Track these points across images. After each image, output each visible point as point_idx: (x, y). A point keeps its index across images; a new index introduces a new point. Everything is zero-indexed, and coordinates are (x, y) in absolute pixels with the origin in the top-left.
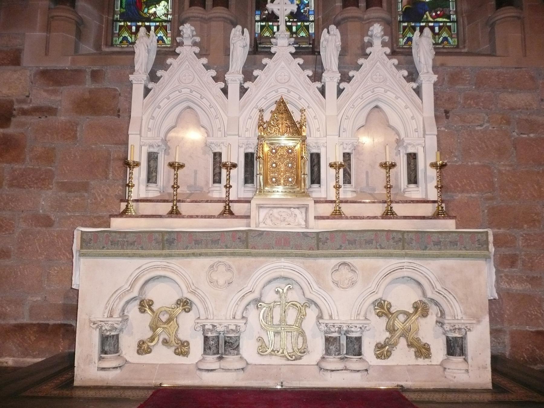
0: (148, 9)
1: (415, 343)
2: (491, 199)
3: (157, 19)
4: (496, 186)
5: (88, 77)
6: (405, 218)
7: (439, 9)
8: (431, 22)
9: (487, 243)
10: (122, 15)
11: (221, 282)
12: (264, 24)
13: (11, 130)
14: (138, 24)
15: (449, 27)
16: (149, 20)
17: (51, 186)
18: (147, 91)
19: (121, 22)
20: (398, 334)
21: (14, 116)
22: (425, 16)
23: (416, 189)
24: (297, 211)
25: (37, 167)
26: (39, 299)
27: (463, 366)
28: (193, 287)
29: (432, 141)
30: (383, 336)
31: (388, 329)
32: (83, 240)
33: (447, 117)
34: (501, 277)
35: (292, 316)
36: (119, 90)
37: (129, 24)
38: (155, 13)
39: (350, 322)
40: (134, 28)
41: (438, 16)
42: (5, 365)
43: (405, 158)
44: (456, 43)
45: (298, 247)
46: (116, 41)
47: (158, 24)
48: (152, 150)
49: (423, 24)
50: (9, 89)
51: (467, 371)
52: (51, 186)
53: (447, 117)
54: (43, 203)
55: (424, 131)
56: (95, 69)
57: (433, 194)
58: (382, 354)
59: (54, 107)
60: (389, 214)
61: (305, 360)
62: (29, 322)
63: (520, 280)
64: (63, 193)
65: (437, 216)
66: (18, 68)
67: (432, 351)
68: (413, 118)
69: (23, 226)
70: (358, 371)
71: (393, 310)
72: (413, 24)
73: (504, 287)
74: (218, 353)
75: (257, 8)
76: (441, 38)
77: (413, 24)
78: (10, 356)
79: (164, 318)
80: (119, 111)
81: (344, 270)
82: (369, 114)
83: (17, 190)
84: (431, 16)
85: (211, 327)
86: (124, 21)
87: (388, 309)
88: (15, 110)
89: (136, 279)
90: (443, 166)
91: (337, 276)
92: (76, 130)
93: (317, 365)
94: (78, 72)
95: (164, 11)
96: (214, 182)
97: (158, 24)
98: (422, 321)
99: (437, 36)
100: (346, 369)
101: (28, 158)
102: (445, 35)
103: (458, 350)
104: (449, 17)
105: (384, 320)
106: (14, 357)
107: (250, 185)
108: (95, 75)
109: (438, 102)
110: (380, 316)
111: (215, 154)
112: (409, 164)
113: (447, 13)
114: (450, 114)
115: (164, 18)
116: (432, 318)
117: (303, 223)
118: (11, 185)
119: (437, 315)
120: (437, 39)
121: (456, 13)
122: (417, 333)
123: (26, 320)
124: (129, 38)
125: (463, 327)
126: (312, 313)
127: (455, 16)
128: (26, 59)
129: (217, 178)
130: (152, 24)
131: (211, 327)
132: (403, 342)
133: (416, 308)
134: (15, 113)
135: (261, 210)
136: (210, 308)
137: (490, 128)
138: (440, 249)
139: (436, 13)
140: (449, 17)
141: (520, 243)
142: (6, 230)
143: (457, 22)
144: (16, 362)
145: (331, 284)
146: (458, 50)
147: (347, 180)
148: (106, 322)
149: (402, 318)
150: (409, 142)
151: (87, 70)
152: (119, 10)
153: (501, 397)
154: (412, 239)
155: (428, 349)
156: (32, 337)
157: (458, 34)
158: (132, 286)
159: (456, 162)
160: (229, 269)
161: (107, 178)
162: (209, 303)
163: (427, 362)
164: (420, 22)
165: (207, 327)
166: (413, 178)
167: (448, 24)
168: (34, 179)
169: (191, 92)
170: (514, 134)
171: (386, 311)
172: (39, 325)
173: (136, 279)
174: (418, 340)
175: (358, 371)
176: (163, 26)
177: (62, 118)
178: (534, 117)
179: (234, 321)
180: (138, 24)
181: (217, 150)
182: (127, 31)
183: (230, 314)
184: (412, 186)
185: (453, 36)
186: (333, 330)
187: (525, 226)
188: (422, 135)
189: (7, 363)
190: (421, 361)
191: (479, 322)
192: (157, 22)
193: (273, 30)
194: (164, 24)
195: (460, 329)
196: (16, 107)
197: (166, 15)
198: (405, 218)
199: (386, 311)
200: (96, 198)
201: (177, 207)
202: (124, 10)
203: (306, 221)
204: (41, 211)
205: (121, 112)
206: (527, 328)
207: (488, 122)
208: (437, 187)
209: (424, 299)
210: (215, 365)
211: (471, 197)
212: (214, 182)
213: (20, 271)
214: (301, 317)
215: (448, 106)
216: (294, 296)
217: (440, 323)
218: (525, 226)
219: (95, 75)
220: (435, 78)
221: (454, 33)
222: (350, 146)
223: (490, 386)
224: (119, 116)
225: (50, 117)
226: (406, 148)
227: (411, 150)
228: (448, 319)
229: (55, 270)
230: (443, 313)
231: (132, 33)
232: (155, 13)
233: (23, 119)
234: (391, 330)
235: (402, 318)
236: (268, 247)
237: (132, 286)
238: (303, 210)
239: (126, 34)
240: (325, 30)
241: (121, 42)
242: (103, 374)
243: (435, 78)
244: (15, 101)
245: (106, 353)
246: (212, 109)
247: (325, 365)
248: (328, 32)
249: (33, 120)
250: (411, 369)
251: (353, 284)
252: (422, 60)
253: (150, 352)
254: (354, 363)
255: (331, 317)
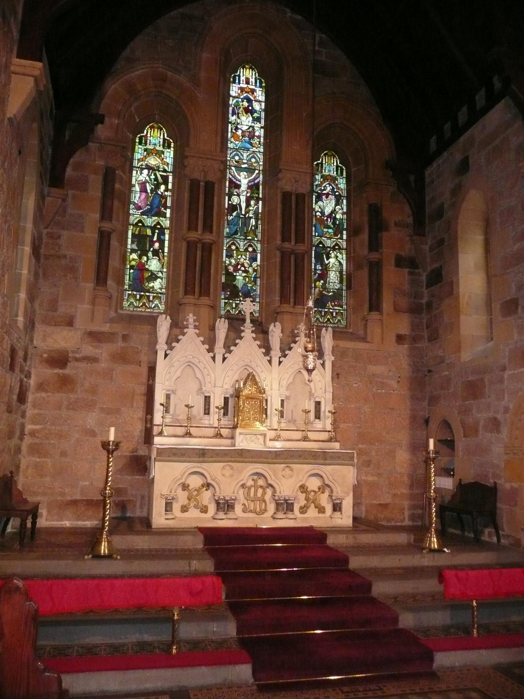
0: (148, 284)
1: (319, 507)
2: (360, 427)
3: (154, 292)
4: (363, 420)
5: (120, 339)
6: (315, 441)
7: (336, 300)
8: (332, 309)
9: (353, 457)
10: (130, 285)
11: (227, 475)
12: (227, 301)
13: (67, 371)
14: (141, 294)
15: (342, 313)
16: (149, 292)
17: (95, 410)
18: (166, 355)
19: (129, 291)
20: (311, 501)
21: (70, 362)
22: (328, 305)
23: (319, 422)
24: (260, 437)
25: (86, 397)
26: (88, 483)
27: (340, 516)
28: (214, 477)
29: (329, 396)
30: (303, 503)
31: (306, 499)
32: (157, 453)
33: (338, 378)
34: (362, 473)
35: (260, 491)
36: (140, 348)
37: (135, 293)
38: (153, 287)
39: (289, 495)
40: (138, 297)
41: (335, 305)
42: (64, 526)
43: (314, 403)
44: (345, 324)
45: (266, 458)
46: (125, 304)
47: (155, 295)
48: (168, 393)
49: (327, 310)
50: (66, 343)
51: (342, 518)
52: (95, 410)
53: (338, 378)
54: (90, 421)
55: (325, 390)
56: (125, 333)
57: (329, 427)
58: (303, 511)
59: (97, 357)
60: (305, 439)
61: (266, 515)
62: (80, 498)
63: (373, 475)
64: (103, 415)
65: (330, 440)
66: (71, 328)
67: (326, 510)
68: (320, 381)
69: (77, 436)
70: (292, 519)
71: (309, 490)
72: (320, 310)
73: (364, 478)
74: (224, 511)
75: (223, 291)
76: (337, 320)
77: (320, 310)
78: (68, 520)
79: (195, 493)
80: (140, 362)
81: (287, 470)
82: (295, 375)
83: (72, 412)
84: (332, 305)
85: (223, 498)
86: (132, 291)
87: (307, 489)
88: (70, 357)
89: (184, 473)
90: (334, 413)
91: (284, 473)
92: (113, 374)
93: (272, 517)
94: (113, 334)
95: (159, 286)
96: (205, 414)
97: (155, 295)
98: (322, 495)
99: (334, 319)
100: (287, 518)
101: (79, 391)
102: (339, 318)
103: (338, 509)
104: (342, 307)
105: (304, 495)
106: (70, 521)
107: (227, 417)
108: (125, 338)
109: (334, 368)
110: (302, 493)
111: (206, 397)
112: (316, 407)
113: (341, 303)
114: (340, 376)
115: (159, 291)
116: (327, 494)
117: (263, 443)
118: (68, 408)
119: (329, 492)
120: (334, 321)
121: (346, 304)
122: (319, 501)
123: (78, 497)
124: (134, 302)
125: (341, 498)
126: (269, 491)
127: (345, 306)
128: (78, 322)
129: (207, 411)
130: (151, 294)
131: (223, 498)
132: (313, 505)
133: (319, 489)
134: (70, 359)
135: (241, 435)
136: (222, 488)
137: (361, 386)
138: (333, 460)
139: (334, 303)
140: (342, 307)
141: (373, 453)
142: (65, 438)
143: (346, 310)
144: (71, 524)
145: (281, 476)
146: (346, 330)
147: (282, 416)
148: (169, 495)
149: (312, 494)
150: (317, 395)
151: (119, 333)
152: (128, 282)
153: (354, 529)
154: (320, 455)
155: (324, 509)
156: (82, 508)
157: (346, 318)
158: (182, 476)
159: (341, 405)
160: (232, 468)
161: (132, 407)
162: (221, 486)
163: (323, 515)
164: (325, 308)
165: (221, 498)
166: (318, 416)
167: (341, 311)
168: (83, 405)
169: (193, 358)
170: (374, 389)
171: (305, 490)
172: (87, 500)
173: (184, 473)
174: (320, 504)
175: (292, 519)
176: (158, 296)
177: (103, 365)
178: (385, 380)
179: (234, 494)
180: (141, 294)
181: (208, 395)
182: (133, 298)
183: (232, 491)
184: (317, 420)
185: (344, 319)
186: (281, 499)
187: (377, 444)
188: (324, 391)
189: (66, 525)
190: (321, 515)
191: (348, 495)
192: (154, 293)
193: (232, 305)
194: (159, 295)
195: (340, 499)
196: (71, 355)
197: (161, 289)
198: (315, 441)
199: (305, 490)
200: (125, 419)
201: (190, 431)
202: (132, 283)
203: (264, 441)
204: (88, 426)
205: (142, 363)
206: (374, 502)
207: (360, 381)
208: (331, 424)
209: (323, 485)
210: (224, 517)
211: (349, 426)
212: (205, 414)
213: (74, 465)
214: (264, 493)
215: (339, 372)
216: (261, 482)
217: (330, 496)
218: (377, 444)
219: (125, 338)
220: (333, 358)
221: (345, 317)
222: (284, 396)
223: (351, 526)
224: (140, 366)
225: (94, 364)
226: (315, 398)
227: (318, 400)
228: (334, 494)
229: (98, 465)
230: (332, 491)
231: (136, 300)
232: (153, 287)
233: (76, 364)
234: (307, 499)
235: (312, 494)
236: (252, 457)
237: (182, 476)
238: (263, 436)
239: (132, 300)
240: (273, 324)
241: (129, 305)
242: (168, 521)
243: (333, 358)
244: (70, 351)
245: (167, 511)
246: (205, 370)
247: (276, 516)
248: (275, 326)
249: (83, 365)
250: (315, 518)
251: (292, 476)
252: (327, 347)
253: (187, 511)
254: (290, 515)
255: (280, 493)
